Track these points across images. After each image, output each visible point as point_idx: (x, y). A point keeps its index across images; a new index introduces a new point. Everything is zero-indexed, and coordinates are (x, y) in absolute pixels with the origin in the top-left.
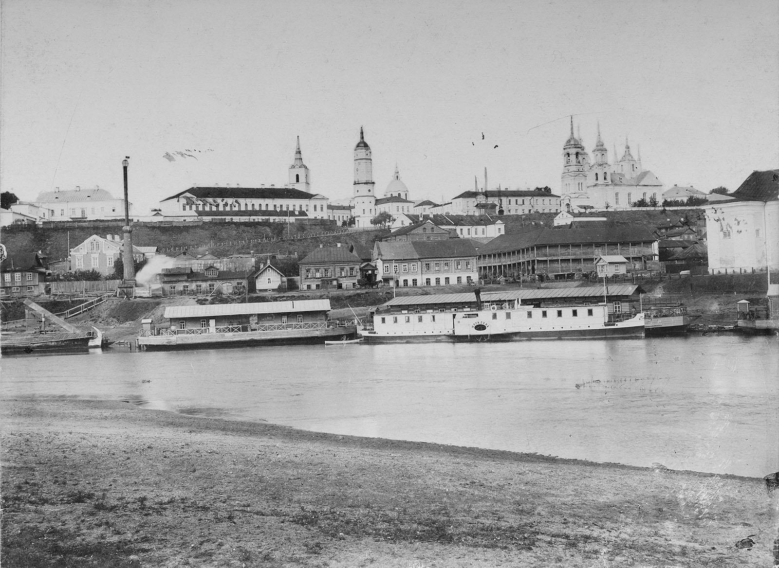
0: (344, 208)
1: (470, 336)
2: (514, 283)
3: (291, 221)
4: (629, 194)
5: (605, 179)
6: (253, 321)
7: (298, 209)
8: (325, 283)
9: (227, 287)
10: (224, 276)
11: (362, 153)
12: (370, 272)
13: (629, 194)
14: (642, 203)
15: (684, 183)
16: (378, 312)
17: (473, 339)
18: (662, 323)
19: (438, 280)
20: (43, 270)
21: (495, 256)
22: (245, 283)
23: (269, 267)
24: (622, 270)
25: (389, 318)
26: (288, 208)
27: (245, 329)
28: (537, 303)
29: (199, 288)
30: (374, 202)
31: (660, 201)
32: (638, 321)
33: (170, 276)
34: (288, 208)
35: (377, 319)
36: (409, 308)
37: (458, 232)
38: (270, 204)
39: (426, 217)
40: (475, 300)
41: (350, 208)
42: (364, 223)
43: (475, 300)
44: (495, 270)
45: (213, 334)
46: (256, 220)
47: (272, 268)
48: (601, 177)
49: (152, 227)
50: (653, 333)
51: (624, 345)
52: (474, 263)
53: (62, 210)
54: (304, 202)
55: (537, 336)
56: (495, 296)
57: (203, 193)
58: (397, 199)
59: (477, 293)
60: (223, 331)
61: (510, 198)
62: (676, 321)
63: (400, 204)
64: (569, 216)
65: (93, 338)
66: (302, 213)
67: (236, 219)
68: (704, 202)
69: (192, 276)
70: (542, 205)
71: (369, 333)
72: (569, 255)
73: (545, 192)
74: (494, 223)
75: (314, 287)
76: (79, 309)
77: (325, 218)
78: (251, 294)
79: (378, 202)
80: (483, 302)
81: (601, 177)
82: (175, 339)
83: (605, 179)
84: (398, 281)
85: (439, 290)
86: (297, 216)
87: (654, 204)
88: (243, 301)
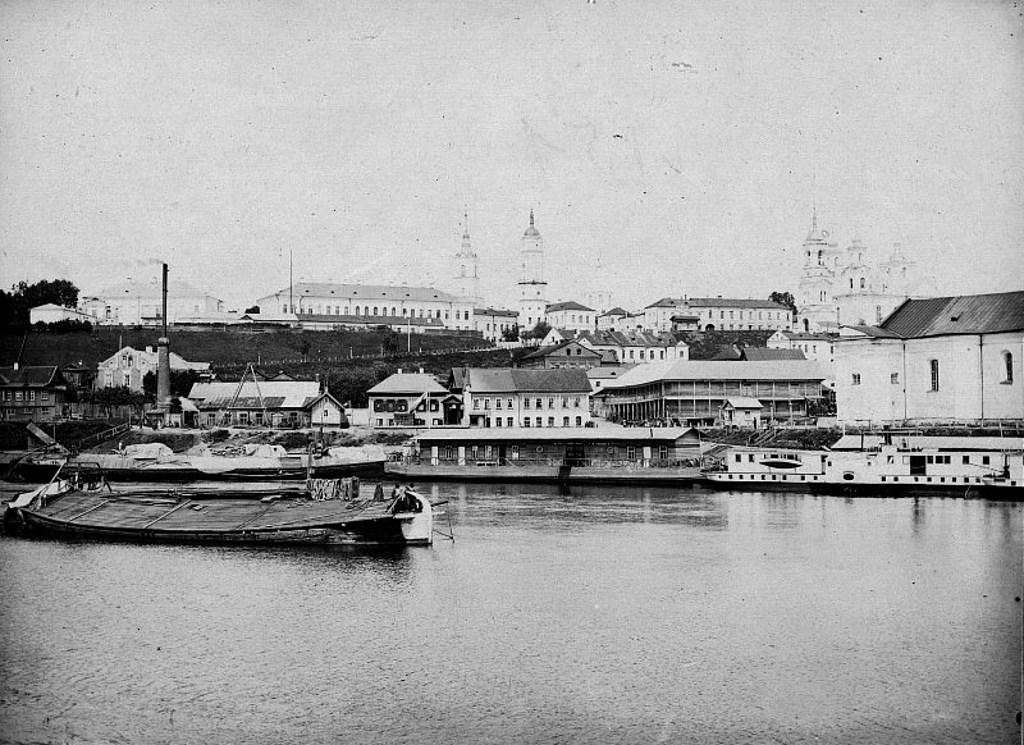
3: (421, 332)
4: (878, 308)
5: (863, 286)
11: (530, 243)
12: (454, 407)
13: (878, 308)
30: (544, 309)
48: (857, 283)
51: (933, 506)
53: (338, 307)
55: (133, 537)
61: (722, 309)
72: (707, 395)
81: (857, 283)
83: (863, 286)
84: (489, 419)
86: (428, 325)
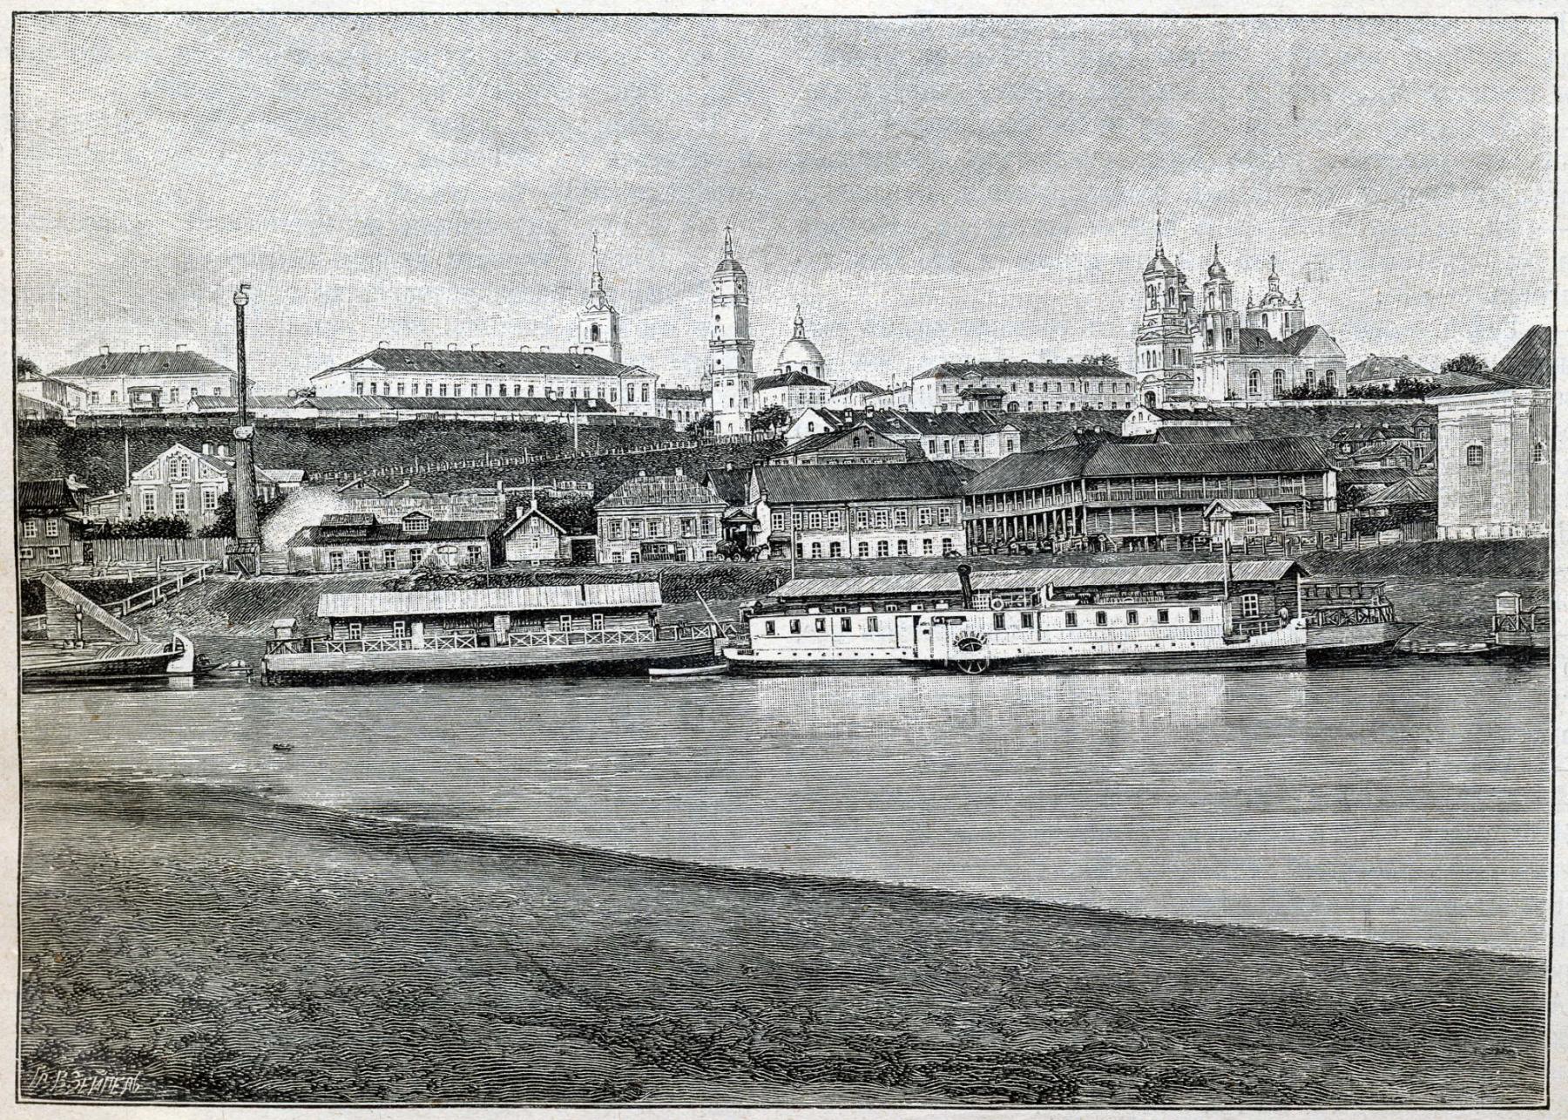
0: (688, 395)
1: (991, 660)
2: (1036, 558)
6: (501, 624)
7: (594, 395)
8: (650, 551)
9: (451, 556)
10: (441, 533)
12: (743, 528)
14: (1302, 393)
15: (1389, 349)
16: (760, 611)
17: (953, 668)
18: (1346, 637)
19: (884, 545)
20: (78, 515)
21: (1068, 489)
22: (484, 547)
23: (534, 514)
24: (1264, 528)
25: (783, 624)
26: (574, 393)
27: (484, 641)
28: (1087, 595)
29: (416, 555)
31: (1341, 387)
32: (1292, 634)
33: (327, 533)
34: (574, 393)
35: (758, 625)
36: (823, 602)
37: (926, 447)
38: (540, 385)
39: (857, 415)
40: (959, 587)
41: (704, 395)
42: (732, 425)
43: (959, 587)
44: (1050, 520)
45: (421, 648)
46: (510, 419)
47: (539, 516)
49: (289, 429)
50: (1319, 660)
52: (961, 512)
54: (609, 382)
56: (1001, 580)
57: (390, 359)
58: (802, 379)
59: (964, 573)
60: (534, 642)
62: (1373, 634)
63: (807, 389)
64: (1154, 417)
65: (176, 657)
66: (601, 405)
67: (464, 415)
68: (1435, 389)
69: (375, 532)
70: (1095, 395)
71: (739, 653)
73: (1098, 369)
74: (999, 430)
75: (627, 558)
76: (148, 596)
77: (652, 413)
78: (498, 573)
79: (763, 384)
80: (976, 591)
82: (354, 661)
85: (910, 566)
87: (1329, 393)
88: (480, 585)
